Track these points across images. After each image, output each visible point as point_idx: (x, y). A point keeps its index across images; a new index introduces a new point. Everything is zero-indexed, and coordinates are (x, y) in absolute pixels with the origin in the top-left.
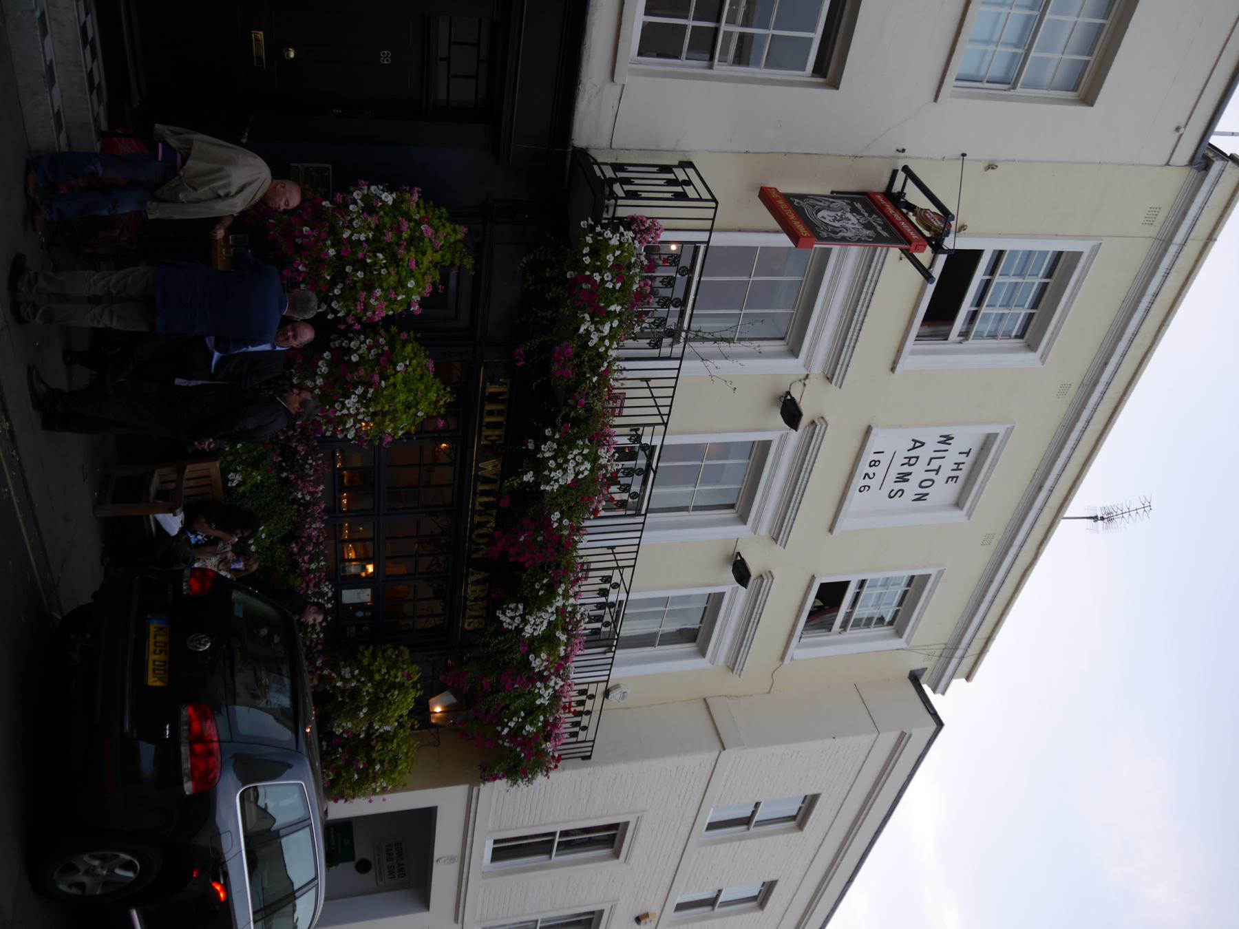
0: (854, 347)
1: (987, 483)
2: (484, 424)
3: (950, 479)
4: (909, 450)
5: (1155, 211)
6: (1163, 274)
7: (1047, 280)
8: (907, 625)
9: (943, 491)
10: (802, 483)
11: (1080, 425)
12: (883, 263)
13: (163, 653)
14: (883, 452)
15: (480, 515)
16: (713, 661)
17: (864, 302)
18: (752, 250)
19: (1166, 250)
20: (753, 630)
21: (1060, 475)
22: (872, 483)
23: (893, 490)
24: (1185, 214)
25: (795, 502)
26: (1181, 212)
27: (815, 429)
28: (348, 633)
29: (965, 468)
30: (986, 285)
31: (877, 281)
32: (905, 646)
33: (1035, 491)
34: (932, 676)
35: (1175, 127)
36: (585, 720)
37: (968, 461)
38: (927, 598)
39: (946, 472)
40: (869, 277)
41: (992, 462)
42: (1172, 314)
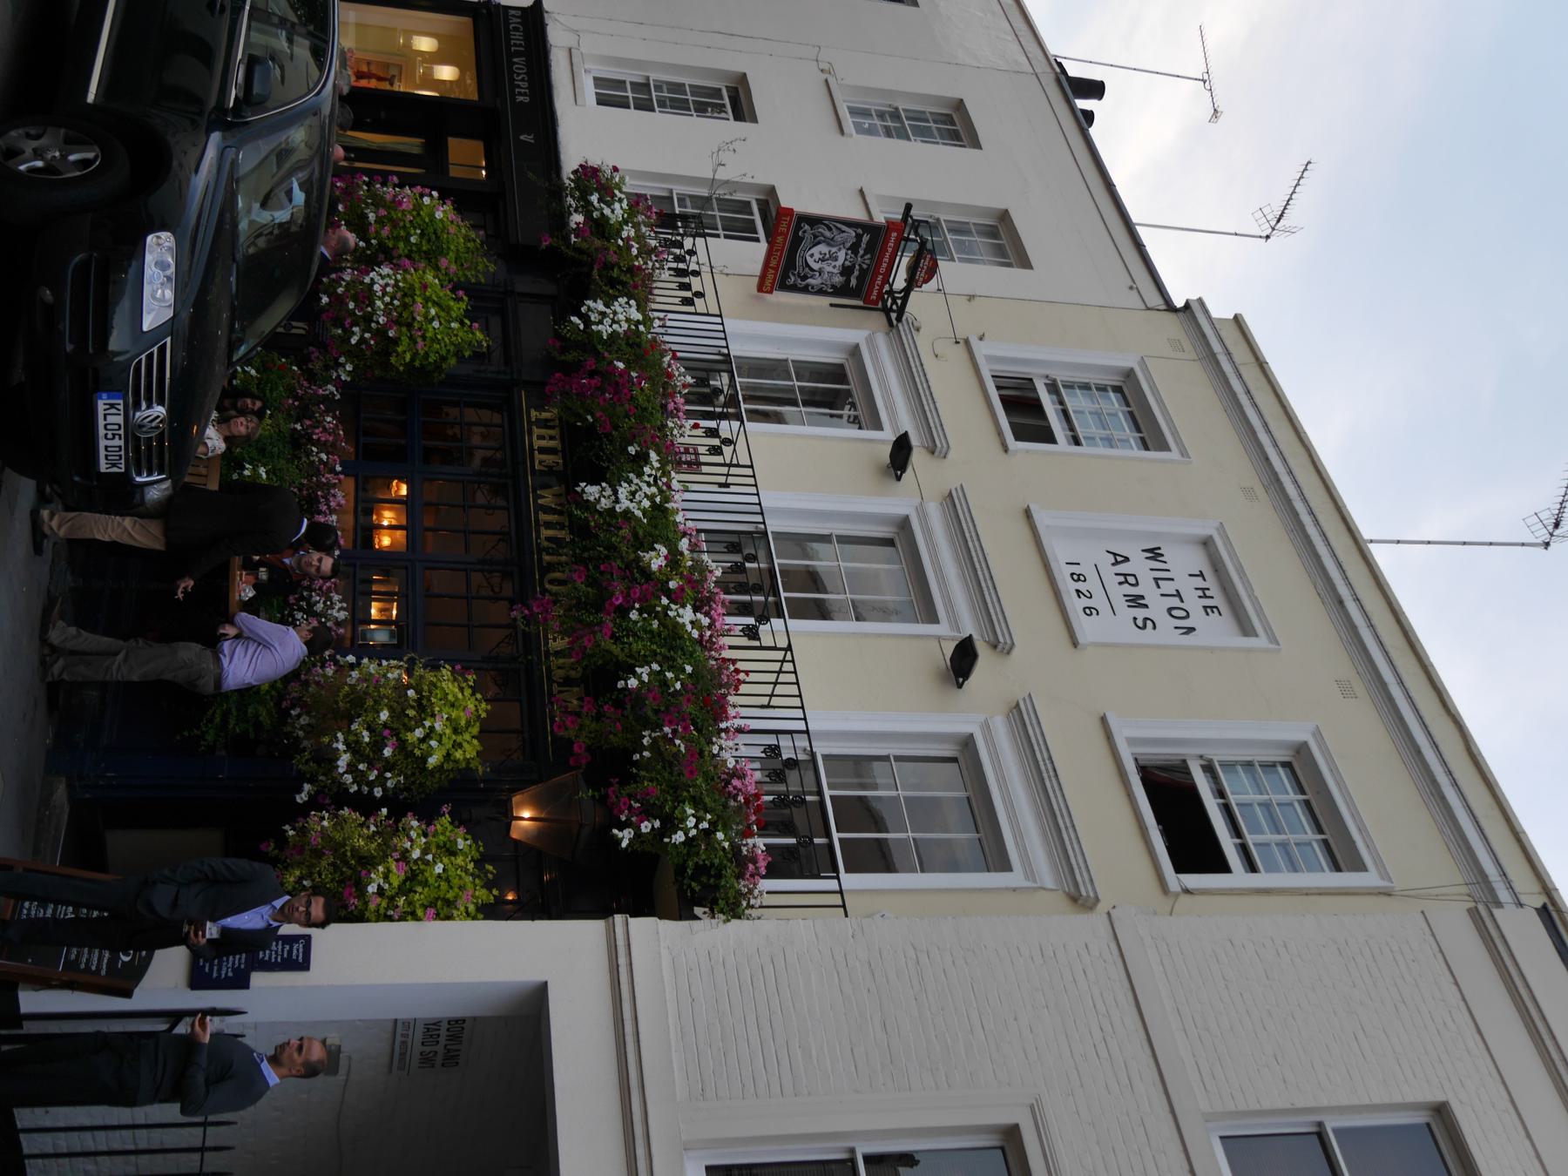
3: (1209, 610)
8: (1354, 842)
11: (1306, 519)
13: (117, 437)
15: (548, 554)
24: (1204, 336)
25: (985, 580)
29: (1214, 591)
31: (941, 425)
35: (1128, 290)
38: (1338, 784)
39: (1193, 603)
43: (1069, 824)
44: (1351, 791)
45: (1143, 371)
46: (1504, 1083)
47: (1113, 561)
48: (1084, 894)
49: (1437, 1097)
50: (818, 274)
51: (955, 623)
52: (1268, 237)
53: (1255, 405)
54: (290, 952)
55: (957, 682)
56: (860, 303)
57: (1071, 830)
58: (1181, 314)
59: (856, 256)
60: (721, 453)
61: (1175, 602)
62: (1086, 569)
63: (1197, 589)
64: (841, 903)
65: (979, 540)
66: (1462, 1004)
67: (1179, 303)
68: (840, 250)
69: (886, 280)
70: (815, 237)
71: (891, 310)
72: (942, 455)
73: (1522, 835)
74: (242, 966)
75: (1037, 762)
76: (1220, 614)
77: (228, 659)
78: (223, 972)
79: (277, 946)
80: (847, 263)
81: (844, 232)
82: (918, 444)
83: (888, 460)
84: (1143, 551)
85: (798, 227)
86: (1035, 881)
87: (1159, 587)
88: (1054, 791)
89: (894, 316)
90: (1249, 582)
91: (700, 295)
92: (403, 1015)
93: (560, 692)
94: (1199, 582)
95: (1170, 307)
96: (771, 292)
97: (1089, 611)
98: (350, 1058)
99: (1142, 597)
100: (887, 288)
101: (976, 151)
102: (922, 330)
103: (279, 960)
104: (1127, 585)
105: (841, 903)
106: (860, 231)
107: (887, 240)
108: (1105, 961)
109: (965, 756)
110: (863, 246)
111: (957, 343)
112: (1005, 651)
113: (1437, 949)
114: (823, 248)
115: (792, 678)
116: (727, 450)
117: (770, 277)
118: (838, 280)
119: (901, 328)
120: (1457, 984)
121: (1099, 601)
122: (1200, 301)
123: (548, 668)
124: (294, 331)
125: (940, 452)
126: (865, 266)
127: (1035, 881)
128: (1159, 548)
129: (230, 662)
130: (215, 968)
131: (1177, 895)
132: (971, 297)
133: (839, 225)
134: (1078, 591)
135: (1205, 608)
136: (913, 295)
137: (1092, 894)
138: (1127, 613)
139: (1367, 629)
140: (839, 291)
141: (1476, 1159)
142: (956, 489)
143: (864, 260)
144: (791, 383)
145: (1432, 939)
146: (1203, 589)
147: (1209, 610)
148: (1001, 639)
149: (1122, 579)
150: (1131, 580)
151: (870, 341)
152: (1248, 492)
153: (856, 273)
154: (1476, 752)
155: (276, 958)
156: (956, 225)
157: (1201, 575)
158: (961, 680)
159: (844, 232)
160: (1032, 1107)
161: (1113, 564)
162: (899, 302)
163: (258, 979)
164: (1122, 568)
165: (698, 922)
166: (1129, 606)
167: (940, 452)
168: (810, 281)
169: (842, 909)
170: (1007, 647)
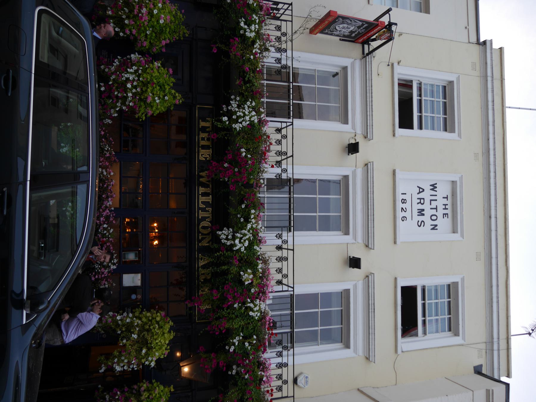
1: (463, 213)
2: (200, 146)
3: (445, 215)
4: (418, 193)
5: (474, 64)
6: (491, 91)
7: (449, 300)
9: (444, 224)
11: (492, 174)
12: (371, 71)
14: (406, 194)
16: (355, 351)
17: (369, 91)
19: (487, 80)
20: (372, 239)
22: (408, 214)
23: (418, 221)
24: (486, 63)
26: (484, 63)
27: (368, 166)
30: (420, 102)
31: (372, 115)
32: (462, 342)
33: (488, 220)
35: (464, 28)
37: (449, 202)
41: (460, 200)
42: (507, 236)
43: (373, 333)
44: (461, 106)
45: (457, 84)
57: (373, 313)
58: (481, 46)
62: (407, 197)
64: (291, 20)
67: (482, 40)
70: (343, 22)
73: (509, 318)
76: (448, 218)
77: (65, 337)
82: (360, 133)
88: (372, 318)
94: (445, 201)
101: (429, 15)
102: (375, 57)
104: (420, 204)
105: (291, 20)
109: (345, 295)
114: (345, 25)
115: (289, 18)
123: (198, 274)
129: (66, 337)
133: (356, 20)
134: (402, 208)
139: (495, 231)
149: (419, 201)
151: (353, 64)
152: (476, 155)
154: (508, 283)
157: (447, 198)
169: (292, 251)
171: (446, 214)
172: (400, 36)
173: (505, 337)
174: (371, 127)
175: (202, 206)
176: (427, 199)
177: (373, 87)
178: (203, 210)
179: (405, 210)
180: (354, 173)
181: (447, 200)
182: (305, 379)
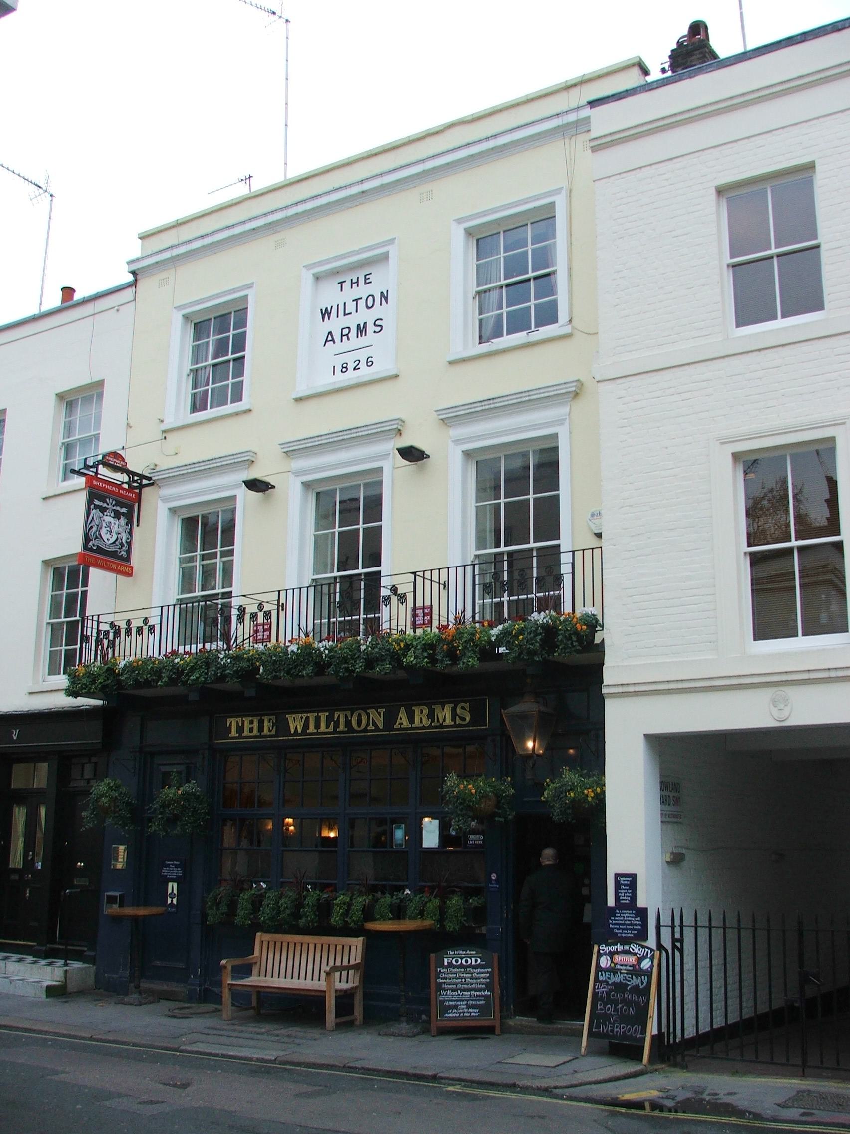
0: (220, 458)
1: (357, 249)
2: (259, 734)
3: (367, 281)
10: (364, 431)
11: (300, 208)
14: (334, 367)
18: (495, 500)
21: (533, 123)
28: (477, 842)
34: (357, 203)
36: (137, 623)
39: (362, 291)
40: (178, 473)
46: (703, 150)
47: (332, 342)
48: (574, 389)
49: (713, 192)
50: (119, 535)
51: (385, 456)
52: (52, 195)
53: (213, 233)
54: (625, 885)
55: (426, 458)
56: (137, 504)
57: (495, 401)
58: (139, 277)
59: (108, 508)
60: (270, 612)
61: (362, 303)
62: (338, 362)
63: (352, 287)
65: (321, 436)
66: (654, 167)
68: (104, 520)
69: (119, 486)
70: (97, 537)
71: (140, 484)
72: (254, 455)
74: (634, 912)
75: (482, 410)
78: (638, 923)
79: (621, 893)
80: (112, 515)
81: (93, 518)
83: (261, 493)
84: (323, 321)
85: (91, 549)
86: (565, 420)
87: (350, 313)
89: (145, 482)
90: (348, 253)
91: (146, 621)
92: (658, 818)
93: (438, 721)
94: (347, 286)
95: (134, 284)
96: (132, 567)
97: (369, 363)
98: (675, 847)
99: (358, 326)
100: (126, 486)
103: (630, 891)
104: (349, 335)
106: (92, 506)
107: (98, 487)
108: (629, 388)
110: (101, 504)
111: (165, 438)
112: (402, 424)
113: (618, 176)
114: (103, 532)
115: (435, 573)
116: (267, 608)
117: (123, 568)
118: (123, 521)
119: (157, 478)
120: (640, 168)
121: (362, 356)
122: (129, 263)
124: (175, 892)
125: (253, 457)
126: (114, 502)
127: (565, 420)
128: (321, 310)
130: (635, 927)
131: (573, 328)
132: (129, 426)
134: (354, 369)
135: (365, 283)
136: (130, 467)
137: (574, 384)
138: (370, 337)
140: (130, 522)
141: (750, 176)
142: (282, 448)
143: (110, 504)
144: (198, 556)
145: (612, 178)
146: (352, 283)
147: (367, 281)
148: (395, 426)
149: (345, 338)
150: (345, 332)
151: (165, 500)
153: (118, 508)
155: (629, 893)
156: (66, 431)
157: (341, 283)
158: (425, 456)
159: (93, 518)
160: (722, 443)
161: (334, 343)
162: (136, 478)
163: (641, 903)
164: (337, 337)
165: (605, 642)
166: (365, 335)
167: (253, 457)
168: (124, 541)
170: (400, 423)
171: (365, 279)
172: (131, 425)
173: (564, 95)
174: (235, 457)
175: (331, 729)
176: (344, 321)
177: (179, 465)
178: (337, 724)
179: (358, 362)
180: (297, 473)
181: (344, 282)
182: (595, 517)
